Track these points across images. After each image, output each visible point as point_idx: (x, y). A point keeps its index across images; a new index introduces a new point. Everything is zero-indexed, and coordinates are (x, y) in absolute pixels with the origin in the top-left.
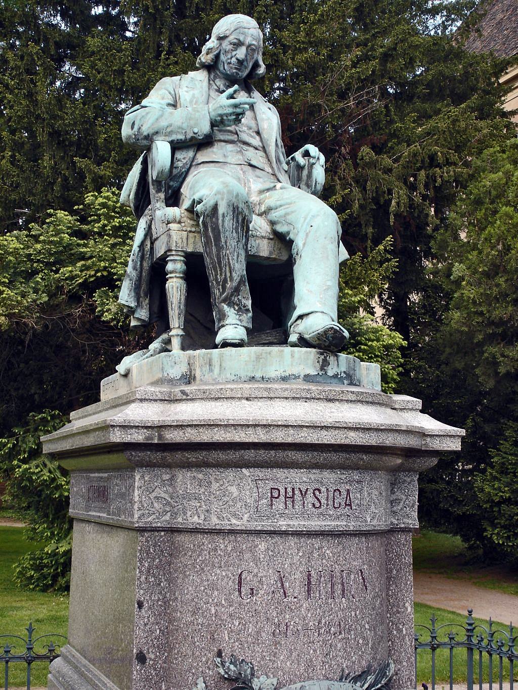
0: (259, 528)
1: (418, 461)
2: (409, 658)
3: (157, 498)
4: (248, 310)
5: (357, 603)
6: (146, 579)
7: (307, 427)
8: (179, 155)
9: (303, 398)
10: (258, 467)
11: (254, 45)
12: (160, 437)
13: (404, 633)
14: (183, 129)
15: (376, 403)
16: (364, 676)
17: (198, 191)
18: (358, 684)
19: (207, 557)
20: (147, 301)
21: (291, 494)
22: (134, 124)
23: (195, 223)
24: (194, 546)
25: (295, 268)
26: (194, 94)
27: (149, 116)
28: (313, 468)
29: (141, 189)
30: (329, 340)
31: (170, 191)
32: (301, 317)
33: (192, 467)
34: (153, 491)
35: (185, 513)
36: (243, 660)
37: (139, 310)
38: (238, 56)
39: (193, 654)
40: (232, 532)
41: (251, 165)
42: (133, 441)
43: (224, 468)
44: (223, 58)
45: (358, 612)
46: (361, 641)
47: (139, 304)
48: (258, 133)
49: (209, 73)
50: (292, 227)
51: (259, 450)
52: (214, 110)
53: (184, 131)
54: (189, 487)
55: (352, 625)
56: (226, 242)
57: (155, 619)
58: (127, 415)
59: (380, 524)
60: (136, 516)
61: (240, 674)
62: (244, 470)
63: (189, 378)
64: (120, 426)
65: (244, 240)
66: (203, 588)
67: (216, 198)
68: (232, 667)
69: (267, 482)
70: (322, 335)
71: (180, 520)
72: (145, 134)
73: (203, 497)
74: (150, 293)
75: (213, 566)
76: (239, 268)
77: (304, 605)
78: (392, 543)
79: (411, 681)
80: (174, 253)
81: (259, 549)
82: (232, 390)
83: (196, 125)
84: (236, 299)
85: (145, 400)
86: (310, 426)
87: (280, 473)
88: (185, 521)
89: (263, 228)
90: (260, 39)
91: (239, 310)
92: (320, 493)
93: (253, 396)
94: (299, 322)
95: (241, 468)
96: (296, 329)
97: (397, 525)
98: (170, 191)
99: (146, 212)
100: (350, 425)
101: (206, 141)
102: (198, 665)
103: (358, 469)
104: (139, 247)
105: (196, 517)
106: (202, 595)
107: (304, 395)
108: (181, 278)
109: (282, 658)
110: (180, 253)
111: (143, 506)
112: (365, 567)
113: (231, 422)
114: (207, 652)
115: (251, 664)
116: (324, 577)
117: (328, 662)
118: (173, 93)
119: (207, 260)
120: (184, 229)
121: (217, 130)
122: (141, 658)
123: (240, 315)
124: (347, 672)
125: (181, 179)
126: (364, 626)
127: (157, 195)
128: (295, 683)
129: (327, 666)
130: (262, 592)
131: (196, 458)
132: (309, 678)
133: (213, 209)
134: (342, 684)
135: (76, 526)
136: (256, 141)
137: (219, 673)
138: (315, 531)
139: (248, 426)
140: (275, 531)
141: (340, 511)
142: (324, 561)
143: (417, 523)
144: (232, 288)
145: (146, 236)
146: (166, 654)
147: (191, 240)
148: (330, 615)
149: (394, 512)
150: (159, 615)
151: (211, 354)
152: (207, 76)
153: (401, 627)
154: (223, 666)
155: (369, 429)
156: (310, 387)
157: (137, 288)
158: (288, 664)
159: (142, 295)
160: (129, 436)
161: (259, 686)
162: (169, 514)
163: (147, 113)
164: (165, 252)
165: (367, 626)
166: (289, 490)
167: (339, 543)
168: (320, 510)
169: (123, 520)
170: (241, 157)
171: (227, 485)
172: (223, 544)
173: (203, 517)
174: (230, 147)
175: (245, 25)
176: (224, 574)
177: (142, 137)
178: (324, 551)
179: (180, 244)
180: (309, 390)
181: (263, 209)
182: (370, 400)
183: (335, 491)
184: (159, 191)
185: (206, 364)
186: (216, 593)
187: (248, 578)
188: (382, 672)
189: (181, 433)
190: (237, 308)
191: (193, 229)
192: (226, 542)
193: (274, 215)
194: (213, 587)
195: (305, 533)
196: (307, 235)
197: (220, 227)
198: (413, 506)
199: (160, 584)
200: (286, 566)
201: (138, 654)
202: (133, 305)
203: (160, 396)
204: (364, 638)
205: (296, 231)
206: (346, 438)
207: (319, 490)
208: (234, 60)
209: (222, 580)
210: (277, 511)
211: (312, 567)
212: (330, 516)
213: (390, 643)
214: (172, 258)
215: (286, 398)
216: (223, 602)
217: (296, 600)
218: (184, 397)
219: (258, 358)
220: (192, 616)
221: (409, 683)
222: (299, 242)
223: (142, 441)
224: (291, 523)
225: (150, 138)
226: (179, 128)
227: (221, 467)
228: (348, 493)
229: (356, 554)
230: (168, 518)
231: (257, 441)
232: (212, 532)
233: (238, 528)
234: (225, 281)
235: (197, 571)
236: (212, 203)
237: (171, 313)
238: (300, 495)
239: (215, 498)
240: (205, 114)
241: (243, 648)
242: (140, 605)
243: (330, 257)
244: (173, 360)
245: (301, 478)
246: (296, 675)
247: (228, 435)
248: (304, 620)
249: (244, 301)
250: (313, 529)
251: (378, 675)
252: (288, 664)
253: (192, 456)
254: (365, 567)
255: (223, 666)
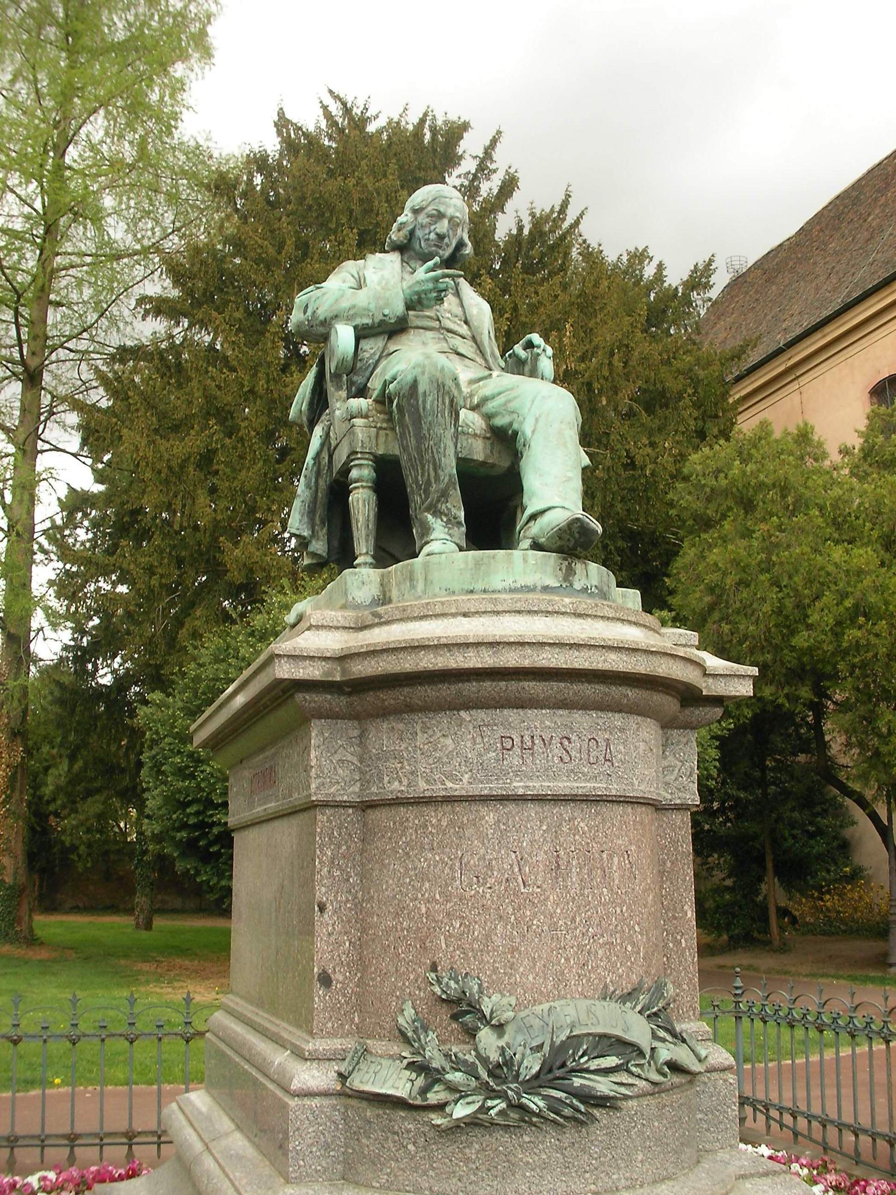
0: (486, 792)
1: (697, 712)
2: (690, 980)
3: (341, 761)
4: (459, 523)
5: (623, 896)
6: (329, 872)
7: (550, 644)
8: (365, 345)
9: (542, 612)
10: (482, 708)
11: (457, 217)
12: (344, 672)
13: (683, 945)
14: (369, 310)
15: (536, 612)
16: (635, 994)
17: (393, 367)
18: (628, 1004)
19: (414, 837)
20: (325, 530)
21: (529, 744)
22: (307, 306)
23: (386, 417)
24: (394, 823)
25: (523, 463)
26: (383, 277)
27: (326, 297)
28: (560, 708)
29: (316, 397)
30: (574, 538)
31: (354, 388)
32: (534, 517)
33: (390, 714)
34: (336, 752)
35: (381, 780)
36: (467, 974)
37: (314, 542)
38: (437, 230)
39: (397, 971)
40: (449, 800)
41: (458, 354)
42: (306, 677)
43: (434, 711)
44: (419, 233)
45: (624, 908)
46: (629, 948)
47: (314, 535)
48: (466, 322)
49: (402, 254)
50: (515, 416)
51: (484, 681)
52: (410, 287)
53: (371, 314)
54: (385, 742)
55: (617, 925)
56: (429, 430)
57: (343, 927)
58: (298, 643)
59: (351, 793)
60: (313, 786)
61: (464, 992)
62: (462, 713)
63: (384, 599)
64: (288, 656)
65: (453, 430)
66: (408, 880)
67: (415, 372)
68: (452, 984)
69: (495, 728)
70: (565, 531)
71: (374, 789)
72: (322, 318)
73: (405, 755)
74: (328, 519)
75: (422, 847)
76: (450, 466)
77: (551, 897)
78: (664, 825)
79: (694, 1010)
80: (359, 456)
81: (487, 822)
82: (443, 603)
83: (387, 305)
84: (444, 507)
85: (323, 627)
86: (554, 644)
87: (512, 715)
88: (381, 790)
89: (477, 424)
90: (464, 211)
91: (449, 522)
92: (570, 743)
93: (472, 610)
94: (532, 523)
95: (458, 710)
96: (527, 534)
97: (671, 801)
98: (354, 388)
99: (323, 417)
100: (610, 643)
101: (399, 327)
102: (404, 984)
103: (620, 711)
104: (314, 459)
105: (396, 783)
106: (408, 889)
107: (543, 608)
108: (369, 487)
109: (521, 969)
110: (367, 456)
111: (322, 772)
112: (633, 848)
113: (443, 641)
114: (416, 967)
115: (478, 978)
116: (578, 859)
117: (585, 975)
118: (356, 276)
119: (403, 463)
120: (372, 425)
121: (414, 316)
122: (326, 980)
123: (449, 529)
124: (612, 989)
125: (367, 374)
126: (633, 927)
127: (336, 394)
128: (541, 1003)
129: (584, 981)
130: (491, 881)
131: (394, 699)
132: (560, 997)
133: (411, 387)
134: (605, 1004)
135: (236, 836)
136: (464, 330)
137: (434, 993)
138: (565, 795)
139: (467, 645)
140: (509, 796)
141: (596, 769)
142: (577, 837)
143: (698, 798)
144: (437, 491)
145: (322, 445)
146: (359, 975)
147: (382, 439)
148: (587, 911)
149: (667, 784)
150: (349, 921)
151: (412, 565)
152: (400, 258)
153: (679, 937)
154: (439, 982)
155: (636, 650)
156: (552, 597)
157: (311, 512)
158: (531, 978)
159: (317, 521)
160: (301, 671)
161: (490, 1007)
162: (358, 784)
163: (324, 294)
164: (348, 457)
165: (637, 928)
166: (527, 738)
167: (597, 813)
168: (571, 766)
169: (296, 799)
170: (445, 345)
171: (439, 734)
172: (434, 817)
173: (405, 782)
174: (430, 334)
175: (446, 194)
176: (437, 859)
177: (317, 322)
178: (576, 823)
179: (367, 444)
180: (550, 601)
181: (476, 400)
182: (633, 619)
183: (590, 740)
184: (339, 388)
185: (404, 580)
186: (427, 885)
187: (472, 862)
188: (659, 988)
189: (373, 663)
190: (445, 520)
191: (385, 425)
192: (440, 815)
193: (490, 406)
194: (423, 876)
195: (549, 797)
196: (537, 420)
197: (421, 410)
198: (691, 775)
199: (348, 880)
200: (525, 844)
201: (320, 974)
202: (306, 533)
203: (343, 623)
204: (633, 944)
205: (521, 418)
206: (605, 661)
207: (568, 739)
208: (432, 236)
209: (435, 866)
210: (511, 767)
211: (560, 846)
212: (584, 774)
213: (665, 959)
214: (357, 462)
215: (519, 612)
216: (438, 897)
217: (539, 890)
218: (376, 621)
219: (478, 564)
220: (394, 919)
221: (691, 1013)
222: (527, 429)
223: (319, 678)
224: (531, 784)
225: (327, 324)
226: (365, 309)
227: (430, 710)
228: (608, 745)
229: (620, 829)
230: (357, 790)
231: (480, 666)
232: (420, 803)
233: (456, 794)
234: (428, 483)
235: (400, 858)
236: (410, 378)
237: (355, 534)
238: (542, 746)
239: (422, 754)
240: (398, 293)
241: (466, 958)
242: (322, 908)
243: (568, 445)
244: (360, 579)
245: (542, 722)
246: (542, 992)
247: (440, 659)
248: (552, 917)
249: (454, 511)
250: (560, 792)
251: (653, 994)
252: (531, 978)
253: (389, 698)
254: (633, 848)
255: (439, 982)
